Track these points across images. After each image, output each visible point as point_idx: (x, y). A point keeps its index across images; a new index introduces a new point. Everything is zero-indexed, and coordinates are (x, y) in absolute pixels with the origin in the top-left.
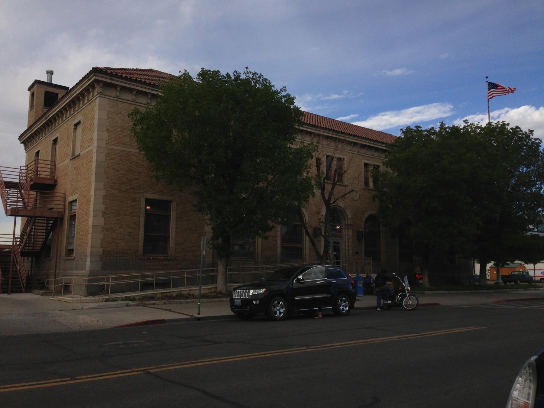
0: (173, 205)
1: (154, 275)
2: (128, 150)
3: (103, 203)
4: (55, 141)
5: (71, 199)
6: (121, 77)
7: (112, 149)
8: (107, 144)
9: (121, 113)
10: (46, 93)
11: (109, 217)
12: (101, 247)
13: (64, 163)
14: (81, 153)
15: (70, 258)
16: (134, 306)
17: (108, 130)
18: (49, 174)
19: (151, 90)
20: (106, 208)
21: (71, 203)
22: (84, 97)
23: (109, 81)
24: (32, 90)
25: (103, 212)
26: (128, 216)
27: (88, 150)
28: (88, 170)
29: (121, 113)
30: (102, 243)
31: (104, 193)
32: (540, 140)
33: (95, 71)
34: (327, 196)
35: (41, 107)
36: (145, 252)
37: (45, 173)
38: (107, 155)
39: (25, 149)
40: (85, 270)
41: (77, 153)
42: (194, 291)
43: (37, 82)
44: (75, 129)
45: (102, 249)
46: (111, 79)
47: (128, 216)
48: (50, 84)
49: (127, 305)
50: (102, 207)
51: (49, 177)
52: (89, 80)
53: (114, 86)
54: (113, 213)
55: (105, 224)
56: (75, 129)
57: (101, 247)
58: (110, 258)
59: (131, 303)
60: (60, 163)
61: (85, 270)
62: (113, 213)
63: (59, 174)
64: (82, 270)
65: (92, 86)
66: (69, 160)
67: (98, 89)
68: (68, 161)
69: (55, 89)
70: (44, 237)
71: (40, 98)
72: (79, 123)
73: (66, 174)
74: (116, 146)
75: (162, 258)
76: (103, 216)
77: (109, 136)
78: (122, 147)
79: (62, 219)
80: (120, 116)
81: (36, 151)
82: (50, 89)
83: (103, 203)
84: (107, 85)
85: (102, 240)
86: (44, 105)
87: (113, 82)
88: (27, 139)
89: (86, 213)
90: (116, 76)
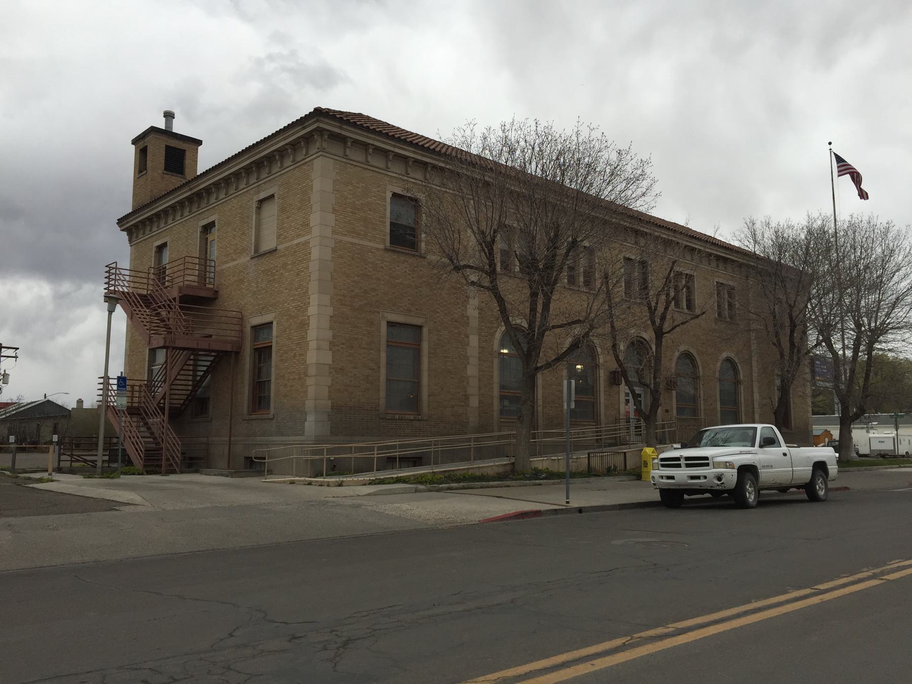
1: (396, 444)
2: (361, 242)
3: (330, 329)
4: (207, 228)
5: (257, 321)
6: (354, 125)
7: (341, 241)
8: (333, 232)
13: (235, 263)
14: (279, 247)
15: (266, 416)
16: (424, 491)
17: (334, 211)
18: (196, 279)
19: (395, 146)
20: (334, 336)
21: (257, 329)
22: (282, 157)
23: (338, 131)
24: (141, 144)
26: (364, 348)
28: (298, 275)
30: (330, 392)
31: (330, 311)
33: (319, 112)
34: (658, 321)
35: (160, 171)
37: (192, 278)
38: (334, 251)
39: (130, 240)
41: (266, 246)
42: (485, 470)
43: (153, 130)
44: (259, 208)
45: (330, 403)
46: (341, 128)
47: (364, 348)
48: (167, 133)
49: (417, 491)
50: (329, 334)
51: (196, 284)
52: (304, 128)
53: (342, 139)
54: (343, 344)
55: (333, 361)
56: (259, 208)
58: (346, 419)
59: (421, 487)
64: (301, 435)
65: (308, 139)
66: (248, 258)
68: (244, 259)
69: (181, 143)
70: (190, 388)
71: (157, 157)
73: (241, 281)
74: (346, 235)
75: (412, 417)
77: (336, 220)
78: (353, 237)
79: (237, 353)
81: (158, 243)
82: (174, 143)
83: (330, 329)
84: (334, 137)
85: (329, 387)
86: (165, 169)
87: (343, 133)
88: (134, 225)
89: (298, 344)
90: (348, 122)
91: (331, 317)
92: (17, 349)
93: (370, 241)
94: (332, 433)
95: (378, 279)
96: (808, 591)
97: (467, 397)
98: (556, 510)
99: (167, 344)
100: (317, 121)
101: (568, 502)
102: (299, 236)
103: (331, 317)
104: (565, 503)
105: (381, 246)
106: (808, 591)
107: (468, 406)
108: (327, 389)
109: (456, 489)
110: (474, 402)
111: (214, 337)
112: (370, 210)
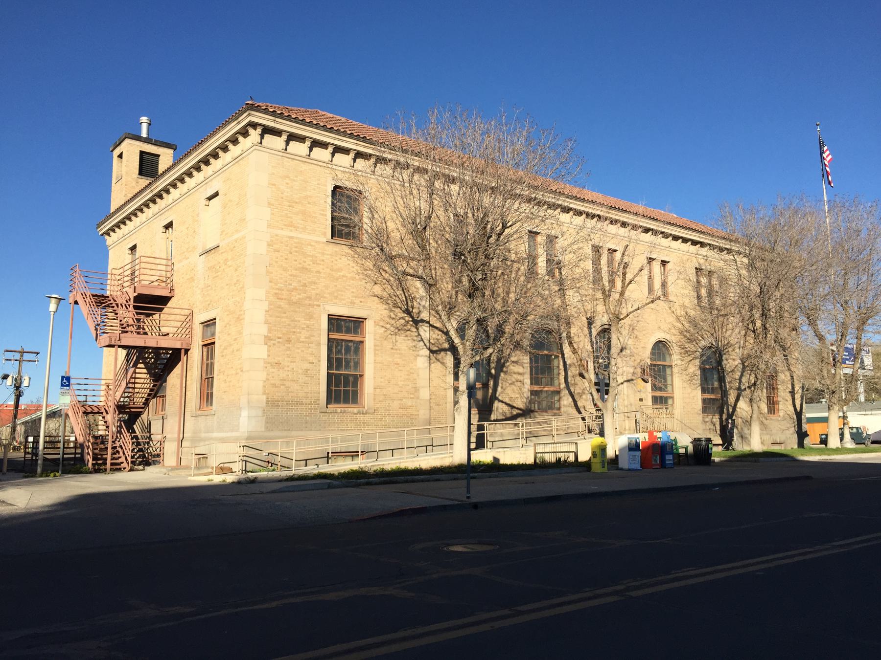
0: (369, 326)
2: (300, 236)
3: (266, 322)
8: (269, 226)
9: (288, 177)
10: (142, 153)
11: (274, 344)
12: (264, 394)
20: (270, 331)
25: (265, 337)
26: (303, 342)
27: (236, 236)
29: (288, 177)
30: (264, 387)
32: (62, 380)
36: (329, 401)
38: (269, 245)
40: (238, 430)
45: (264, 397)
54: (279, 338)
55: (269, 356)
57: (264, 394)
60: (180, 261)
61: (238, 430)
62: (279, 338)
63: (178, 281)
67: (254, 134)
72: (216, 194)
73: (192, 279)
76: (266, 344)
77: (273, 214)
80: (287, 181)
86: (141, 173)
91: (266, 311)
92: (38, 353)
93: (309, 234)
94: (267, 428)
95: (318, 272)
96: (506, 612)
97: (416, 390)
98: (446, 506)
99: (113, 343)
100: (249, 115)
101: (468, 497)
102: (237, 231)
103: (266, 311)
104: (465, 499)
105: (325, 240)
106: (506, 612)
107: (418, 398)
108: (261, 384)
109: (376, 484)
110: (424, 394)
111: (171, 335)
112: (309, 203)
